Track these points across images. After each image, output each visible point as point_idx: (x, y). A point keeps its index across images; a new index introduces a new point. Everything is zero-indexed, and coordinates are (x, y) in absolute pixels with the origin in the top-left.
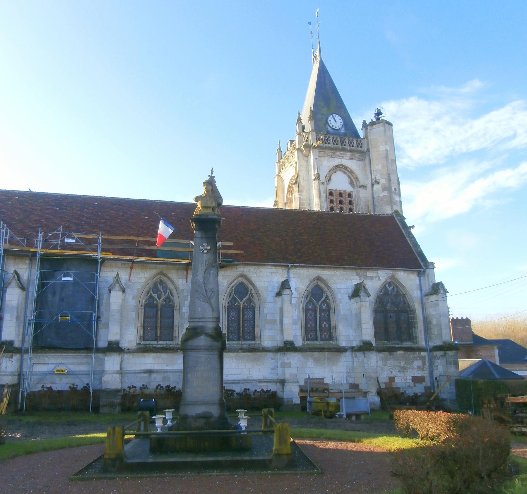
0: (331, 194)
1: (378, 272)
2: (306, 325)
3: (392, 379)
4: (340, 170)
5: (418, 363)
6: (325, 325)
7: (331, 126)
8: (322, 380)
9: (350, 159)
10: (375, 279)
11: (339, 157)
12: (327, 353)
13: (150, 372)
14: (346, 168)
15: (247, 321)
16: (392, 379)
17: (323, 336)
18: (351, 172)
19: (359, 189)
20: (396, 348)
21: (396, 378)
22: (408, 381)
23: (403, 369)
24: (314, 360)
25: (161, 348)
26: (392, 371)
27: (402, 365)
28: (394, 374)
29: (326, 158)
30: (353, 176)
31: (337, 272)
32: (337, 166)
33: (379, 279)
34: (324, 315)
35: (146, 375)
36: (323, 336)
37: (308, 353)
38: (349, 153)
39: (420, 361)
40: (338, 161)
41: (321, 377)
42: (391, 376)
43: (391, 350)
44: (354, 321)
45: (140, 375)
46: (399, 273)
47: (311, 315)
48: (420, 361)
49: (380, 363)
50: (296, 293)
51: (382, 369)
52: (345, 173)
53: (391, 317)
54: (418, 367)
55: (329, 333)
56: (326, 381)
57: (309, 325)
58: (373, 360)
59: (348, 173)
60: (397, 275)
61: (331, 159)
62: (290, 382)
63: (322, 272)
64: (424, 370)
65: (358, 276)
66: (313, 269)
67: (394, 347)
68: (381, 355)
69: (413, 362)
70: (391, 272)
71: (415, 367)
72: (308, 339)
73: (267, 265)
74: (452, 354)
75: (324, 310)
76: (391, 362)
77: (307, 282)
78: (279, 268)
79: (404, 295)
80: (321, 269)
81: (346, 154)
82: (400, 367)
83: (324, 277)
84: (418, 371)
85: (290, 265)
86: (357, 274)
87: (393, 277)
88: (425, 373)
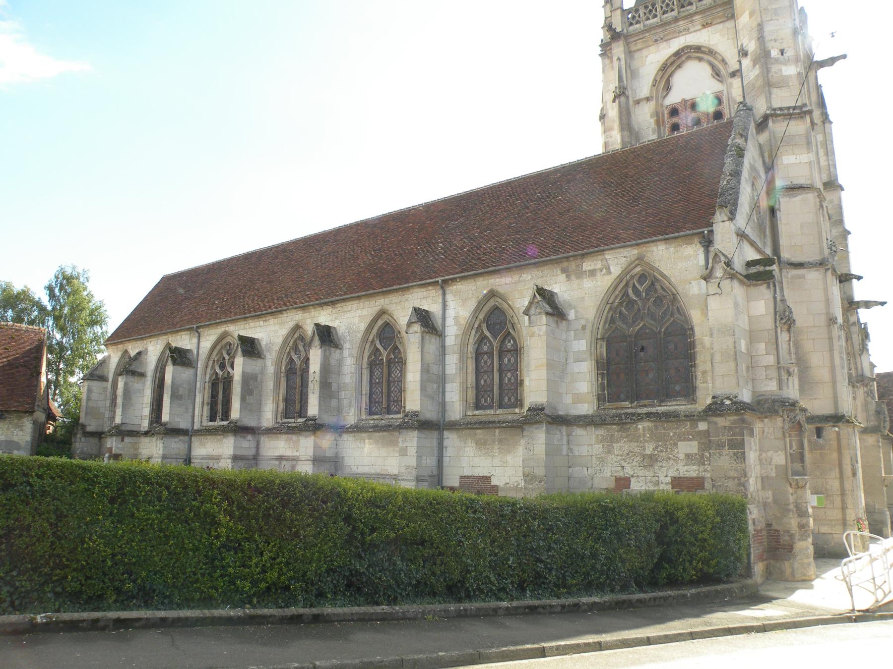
0: (674, 112)
1: (607, 257)
3: (623, 482)
4: (689, 58)
6: (509, 380)
8: (488, 478)
9: (704, 26)
10: (598, 274)
11: (679, 33)
13: (280, 458)
14: (698, 49)
15: (395, 382)
17: (506, 399)
18: (711, 52)
19: (730, 80)
20: (639, 415)
23: (651, 461)
24: (477, 443)
25: (295, 427)
26: (624, 464)
27: (648, 452)
28: (629, 471)
29: (652, 48)
30: (716, 59)
31: (525, 276)
32: (677, 54)
33: (609, 273)
34: (509, 360)
35: (277, 463)
36: (506, 399)
37: (468, 431)
38: (697, 17)
40: (676, 44)
41: (486, 474)
42: (621, 474)
43: (624, 421)
44: (559, 367)
45: (272, 462)
46: (655, 249)
47: (486, 362)
49: (598, 449)
50: (455, 327)
51: (602, 460)
52: (700, 59)
53: (642, 349)
54: (688, 456)
55: (512, 391)
57: (482, 382)
58: (587, 443)
59: (706, 57)
60: (649, 255)
61: (663, 45)
63: (497, 280)
65: (564, 275)
66: (481, 279)
68: (601, 432)
69: (676, 444)
70: (636, 252)
74: (727, 424)
75: (509, 351)
76: (622, 446)
77: (472, 304)
78: (430, 288)
79: (674, 294)
80: (496, 276)
81: (692, 22)
82: (644, 457)
83: (501, 290)
84: (686, 465)
85: (440, 279)
86: (564, 271)
87: (640, 258)
88: (705, 470)
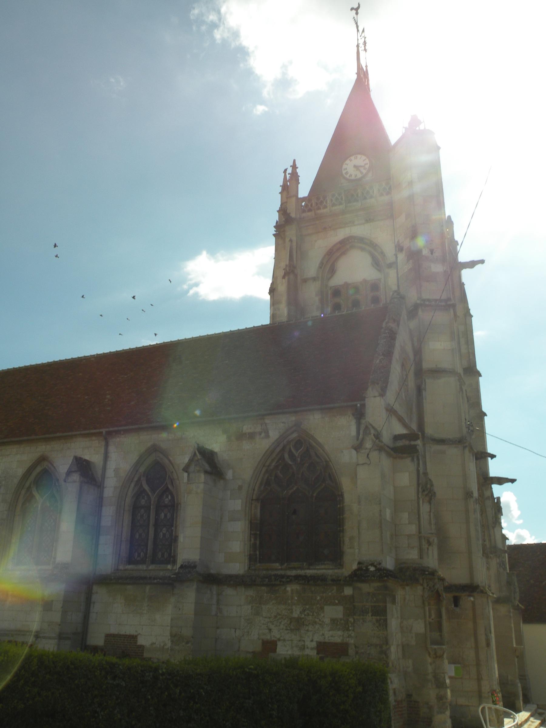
2: (132, 536)
3: (269, 646)
5: (334, 612)
6: (164, 535)
7: (347, 176)
8: (134, 638)
12: (148, 587)
16: (269, 646)
20: (288, 577)
21: (279, 644)
22: (307, 652)
23: (297, 625)
26: (272, 627)
27: (295, 615)
28: (276, 634)
33: (267, 436)
34: (166, 516)
39: (340, 608)
43: (273, 583)
48: (340, 608)
52: (363, 249)
54: (334, 621)
55: (166, 549)
56: (141, 641)
57: (137, 536)
58: (237, 604)
62: (44, 637)
64: (348, 630)
67: (282, 576)
68: (251, 592)
69: (322, 608)
70: (294, 418)
71: (327, 621)
72: (130, 561)
73: (75, 436)
78: (94, 438)
85: (104, 431)
